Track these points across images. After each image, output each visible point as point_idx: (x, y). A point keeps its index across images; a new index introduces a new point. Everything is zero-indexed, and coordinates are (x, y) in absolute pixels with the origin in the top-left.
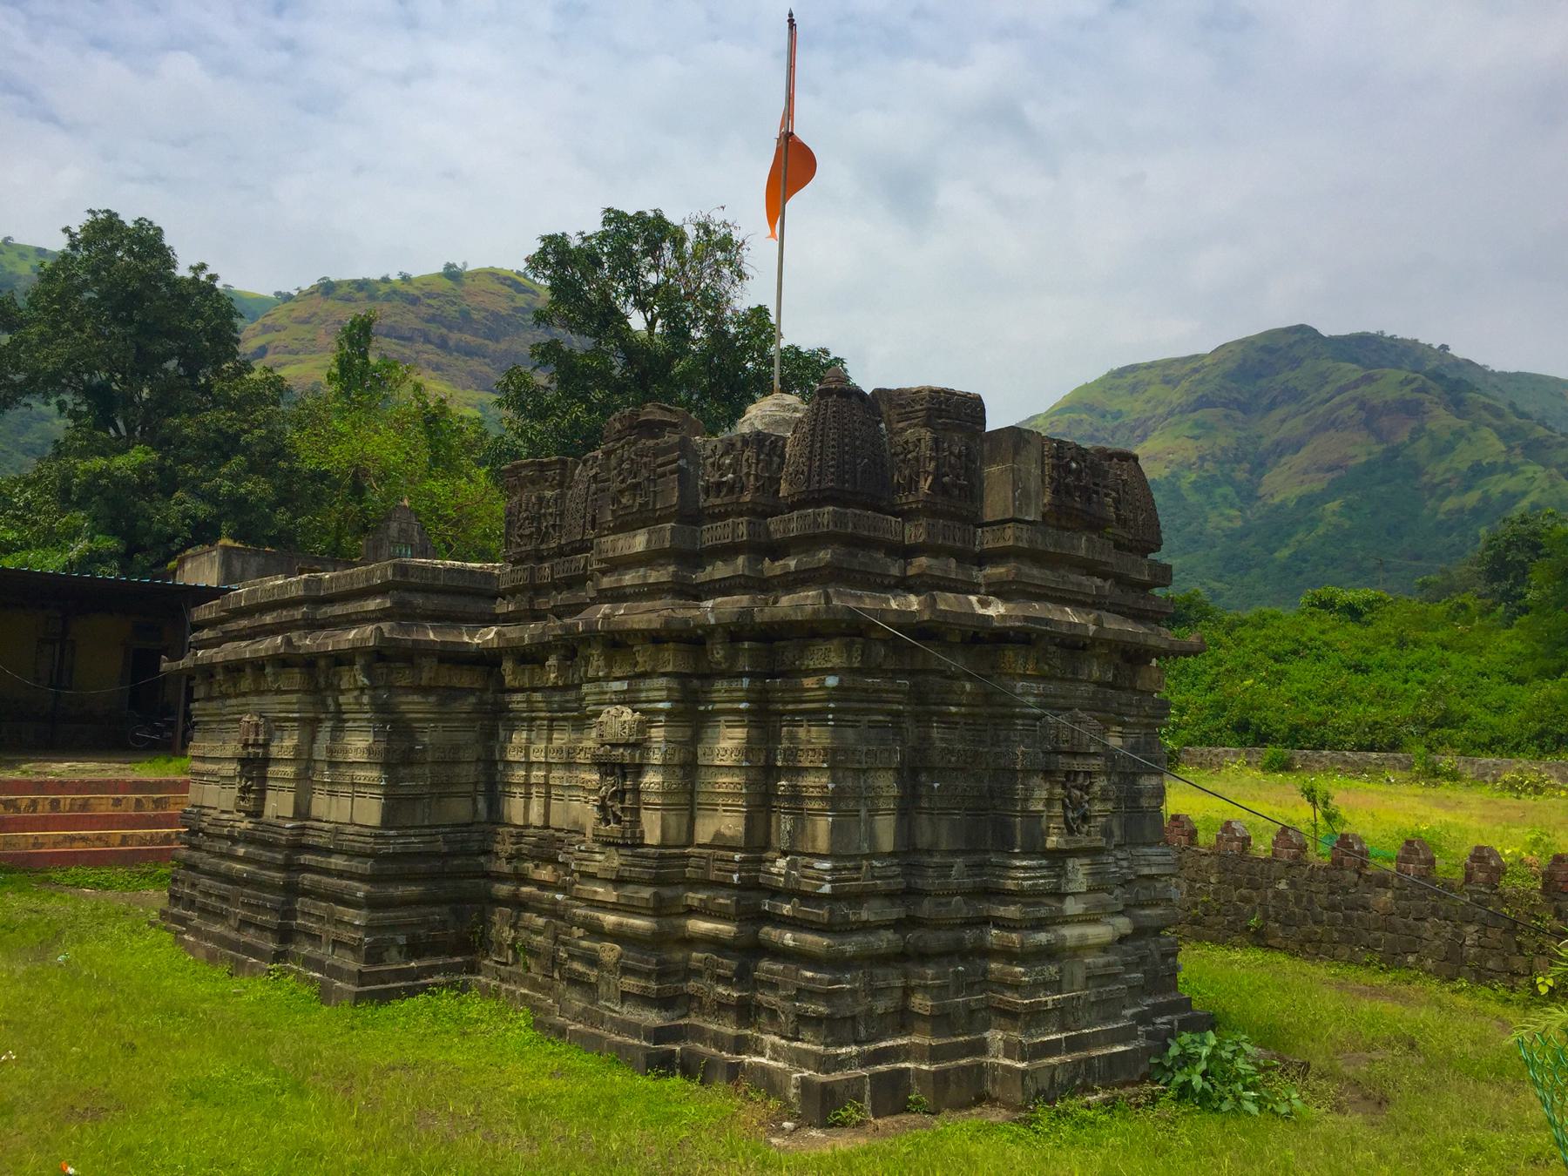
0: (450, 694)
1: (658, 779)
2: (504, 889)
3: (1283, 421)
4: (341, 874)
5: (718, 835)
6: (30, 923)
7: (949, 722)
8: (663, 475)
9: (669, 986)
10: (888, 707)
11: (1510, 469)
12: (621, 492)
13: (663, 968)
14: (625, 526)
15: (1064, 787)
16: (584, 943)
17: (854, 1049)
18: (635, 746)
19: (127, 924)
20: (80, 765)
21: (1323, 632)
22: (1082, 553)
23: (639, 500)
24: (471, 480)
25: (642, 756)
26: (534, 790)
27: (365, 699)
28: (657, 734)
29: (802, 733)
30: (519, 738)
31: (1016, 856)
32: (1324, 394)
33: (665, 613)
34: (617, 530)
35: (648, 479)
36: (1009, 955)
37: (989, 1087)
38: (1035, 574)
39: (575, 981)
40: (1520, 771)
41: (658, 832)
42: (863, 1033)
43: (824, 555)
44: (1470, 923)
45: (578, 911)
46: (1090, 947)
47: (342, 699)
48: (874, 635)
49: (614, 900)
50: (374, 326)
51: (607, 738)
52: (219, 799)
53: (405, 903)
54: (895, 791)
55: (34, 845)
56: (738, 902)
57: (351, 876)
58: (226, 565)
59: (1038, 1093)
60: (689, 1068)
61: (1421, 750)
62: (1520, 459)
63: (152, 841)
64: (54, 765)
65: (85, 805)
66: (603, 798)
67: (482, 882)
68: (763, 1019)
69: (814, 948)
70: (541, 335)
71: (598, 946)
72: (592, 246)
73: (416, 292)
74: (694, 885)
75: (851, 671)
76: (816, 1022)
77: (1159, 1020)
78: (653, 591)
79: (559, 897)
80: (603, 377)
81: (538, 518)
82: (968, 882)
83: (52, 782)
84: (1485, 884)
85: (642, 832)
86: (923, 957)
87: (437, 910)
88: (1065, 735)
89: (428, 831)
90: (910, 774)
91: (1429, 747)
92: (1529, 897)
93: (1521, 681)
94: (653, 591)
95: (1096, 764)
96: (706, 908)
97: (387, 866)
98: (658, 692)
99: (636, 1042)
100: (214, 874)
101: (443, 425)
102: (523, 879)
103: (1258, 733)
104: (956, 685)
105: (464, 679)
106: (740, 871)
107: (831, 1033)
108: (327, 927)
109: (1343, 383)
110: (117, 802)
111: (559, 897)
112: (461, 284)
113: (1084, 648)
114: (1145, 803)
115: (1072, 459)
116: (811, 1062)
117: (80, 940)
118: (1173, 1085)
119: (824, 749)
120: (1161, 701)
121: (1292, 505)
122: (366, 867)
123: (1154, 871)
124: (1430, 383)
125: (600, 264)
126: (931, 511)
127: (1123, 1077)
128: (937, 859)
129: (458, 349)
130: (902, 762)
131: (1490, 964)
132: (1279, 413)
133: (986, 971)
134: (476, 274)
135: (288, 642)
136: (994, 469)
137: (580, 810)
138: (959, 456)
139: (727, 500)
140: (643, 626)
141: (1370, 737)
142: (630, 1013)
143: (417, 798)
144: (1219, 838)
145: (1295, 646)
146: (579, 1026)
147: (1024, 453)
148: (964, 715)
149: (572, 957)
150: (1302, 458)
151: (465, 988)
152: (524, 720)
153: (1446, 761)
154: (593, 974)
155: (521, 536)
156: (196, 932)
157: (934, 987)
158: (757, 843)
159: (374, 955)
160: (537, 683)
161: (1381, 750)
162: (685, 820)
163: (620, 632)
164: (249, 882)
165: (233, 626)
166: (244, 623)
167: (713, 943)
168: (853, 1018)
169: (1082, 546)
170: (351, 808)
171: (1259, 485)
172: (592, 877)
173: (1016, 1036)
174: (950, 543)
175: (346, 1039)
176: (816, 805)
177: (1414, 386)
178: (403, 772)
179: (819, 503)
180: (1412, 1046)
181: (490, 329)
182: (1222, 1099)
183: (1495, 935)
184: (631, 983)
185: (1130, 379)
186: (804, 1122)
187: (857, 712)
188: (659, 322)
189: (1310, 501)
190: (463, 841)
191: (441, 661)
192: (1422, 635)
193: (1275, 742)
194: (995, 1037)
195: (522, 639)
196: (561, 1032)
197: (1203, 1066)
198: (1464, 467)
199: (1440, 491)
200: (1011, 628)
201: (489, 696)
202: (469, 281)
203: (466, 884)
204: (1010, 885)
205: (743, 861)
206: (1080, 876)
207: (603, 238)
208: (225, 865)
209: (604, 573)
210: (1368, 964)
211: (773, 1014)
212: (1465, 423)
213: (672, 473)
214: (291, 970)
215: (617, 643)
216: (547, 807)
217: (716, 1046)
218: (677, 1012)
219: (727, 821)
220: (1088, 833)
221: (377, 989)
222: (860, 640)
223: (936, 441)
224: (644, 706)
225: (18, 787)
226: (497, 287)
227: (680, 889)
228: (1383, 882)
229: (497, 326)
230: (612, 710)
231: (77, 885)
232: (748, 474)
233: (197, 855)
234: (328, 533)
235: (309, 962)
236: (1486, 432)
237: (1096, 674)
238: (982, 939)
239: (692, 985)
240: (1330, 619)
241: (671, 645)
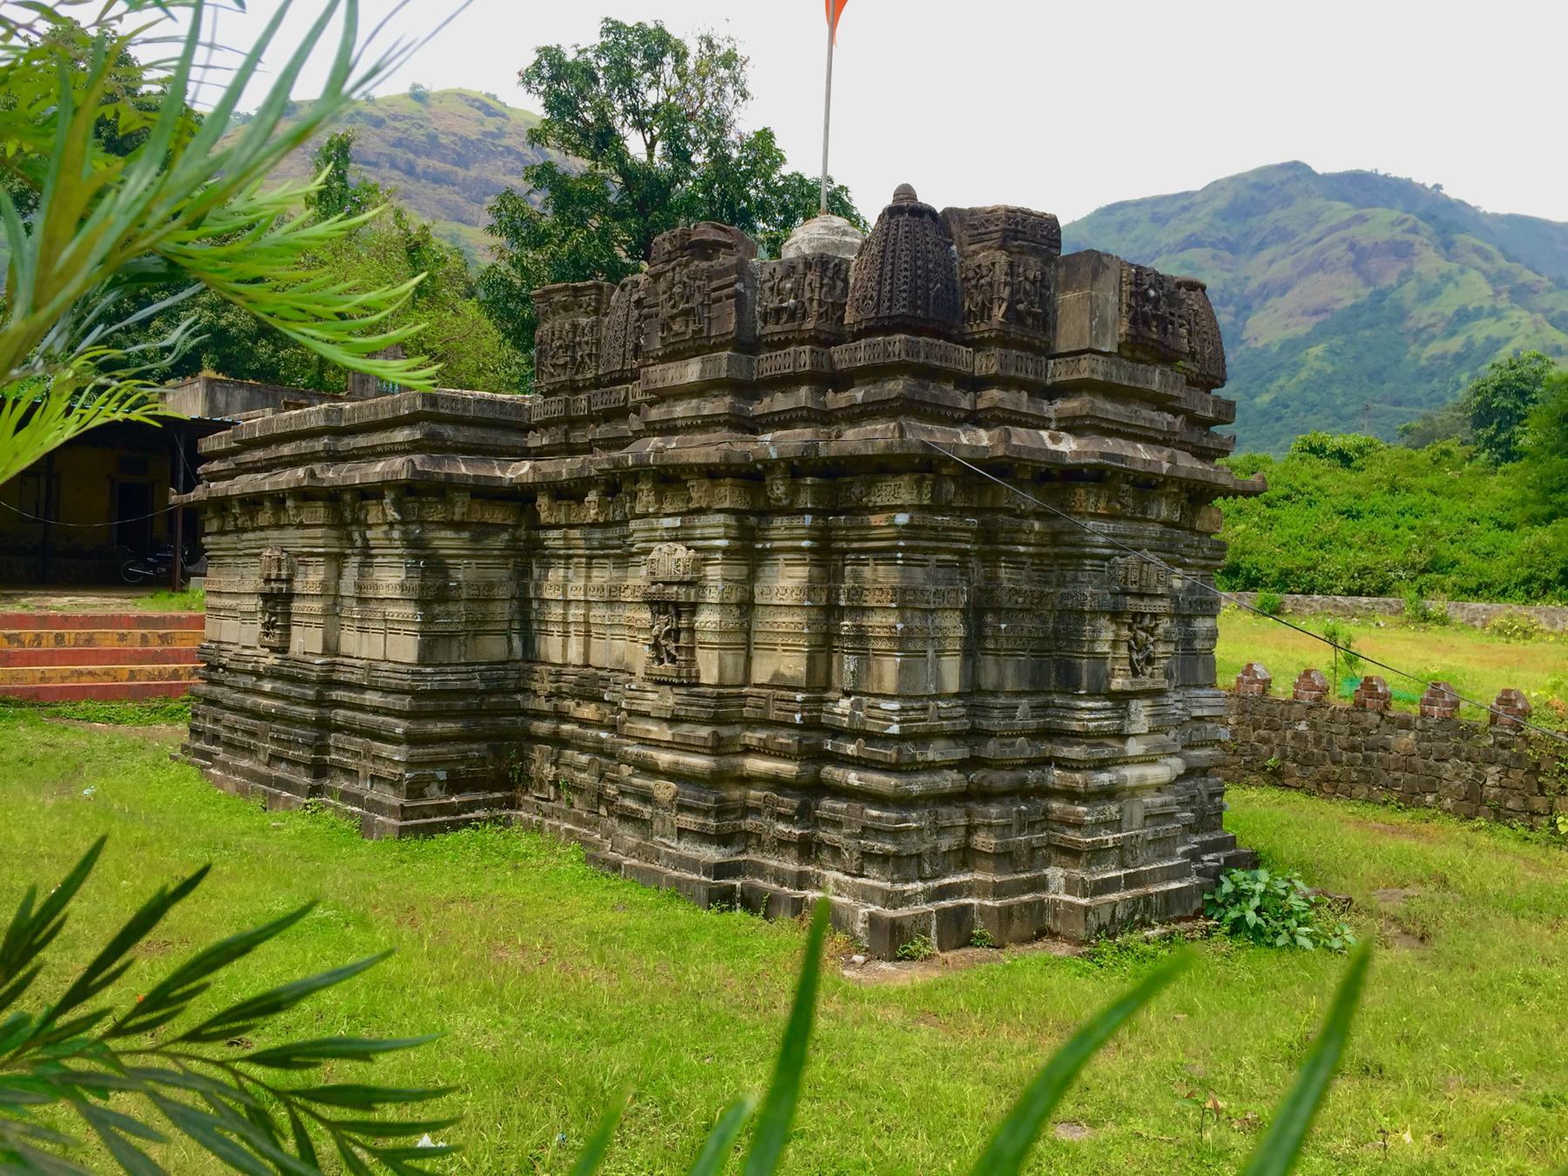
0: (483, 531)
1: (715, 617)
2: (544, 727)
3: (1271, 262)
4: (376, 710)
5: (777, 675)
6: (46, 758)
7: (1015, 560)
8: (719, 300)
9: (729, 823)
10: (955, 546)
11: (1496, 313)
12: (673, 318)
13: (720, 807)
14: (676, 354)
15: (1130, 629)
16: (636, 781)
17: (919, 886)
18: (690, 584)
19: (149, 757)
20: (81, 600)
21: (1316, 477)
22: (1155, 387)
23: (692, 327)
24: (457, 314)
25: (697, 593)
26: (572, 628)
27: (396, 534)
28: (714, 572)
29: (867, 572)
30: (556, 575)
31: (1080, 697)
32: (1314, 234)
33: (725, 446)
34: (665, 359)
35: (702, 304)
36: (1071, 795)
37: (1049, 922)
38: (1109, 409)
39: (627, 817)
40: (1510, 616)
41: (715, 672)
42: (928, 870)
43: (895, 387)
44: (1492, 764)
45: (630, 750)
46: (1148, 787)
47: (369, 534)
48: (944, 471)
49: (669, 738)
50: (353, 146)
51: (660, 576)
52: (241, 634)
53: (443, 739)
54: (961, 632)
55: (41, 679)
56: (800, 741)
57: (388, 712)
58: (210, 397)
59: (1099, 930)
60: (750, 901)
61: (1413, 594)
62: (1507, 304)
63: (160, 676)
64: (54, 600)
65: (89, 641)
66: (656, 637)
67: (519, 719)
68: (825, 855)
69: (880, 788)
70: (534, 157)
71: (651, 784)
72: (587, 61)
73: (382, 115)
74: (750, 724)
75: (921, 508)
76: (885, 858)
77: (1205, 858)
78: (707, 424)
79: (604, 735)
80: (596, 200)
81: (572, 347)
82: (1033, 723)
83: (55, 616)
84: (1510, 726)
85: (698, 672)
86: (987, 796)
87: (476, 746)
88: (1134, 575)
89: (464, 669)
90: (976, 614)
91: (1420, 591)
92: (1555, 739)
93: (1510, 527)
94: (707, 424)
95: (1162, 605)
96: (765, 747)
97: (427, 703)
98: (715, 530)
99: (695, 877)
100: (240, 710)
101: (427, 255)
102: (563, 717)
103: (1248, 578)
104: (1025, 525)
105: (496, 516)
106: (802, 710)
107: (898, 869)
108: (364, 762)
109: (1333, 222)
110: (122, 637)
111: (604, 735)
112: (429, 106)
113: (1154, 487)
114: (1198, 645)
115: (1151, 286)
116: (878, 898)
117: (104, 774)
118: (1226, 920)
119: (893, 588)
120: (1219, 542)
121: (1275, 349)
122: (406, 703)
123: (1206, 712)
124: (1421, 223)
125: (596, 81)
126: (1004, 341)
127: (1178, 913)
128: (1002, 701)
129: (426, 175)
130: (968, 603)
131: (1510, 804)
132: (1266, 254)
133: (1047, 811)
134: (444, 95)
135: (312, 475)
136: (1070, 296)
137: (626, 647)
138: (1033, 283)
139: (787, 327)
140: (700, 460)
141: (1358, 582)
142: (687, 849)
143: (452, 636)
144: (1239, 680)
145: (1287, 491)
146: (634, 861)
147: (1102, 279)
148: (1031, 555)
149: (623, 793)
150: (1289, 301)
151: (507, 823)
152: (559, 557)
153: (1436, 605)
154: (647, 811)
155: (554, 366)
156: (224, 766)
157: (999, 825)
158: (818, 685)
159: (415, 790)
160: (574, 520)
161: (1369, 594)
162: (742, 660)
163: (674, 466)
164: (274, 718)
165: (247, 457)
166: (259, 454)
167: (776, 783)
168: (919, 856)
169: (1155, 379)
170: (387, 643)
171: (1244, 328)
172: (645, 715)
173: (1078, 873)
174: (1022, 375)
175: (398, 871)
176: (883, 645)
177: (1405, 227)
178: (437, 609)
179: (888, 331)
180: (1444, 882)
181: (459, 155)
182: (1276, 934)
183: (1517, 776)
184: (689, 820)
185: (1118, 217)
186: (873, 954)
187: (925, 550)
188: (659, 145)
189: (1293, 346)
190: (498, 679)
191: (473, 496)
192: (1412, 480)
193: (1265, 585)
194: (1056, 874)
195: (560, 473)
196: (616, 867)
197: (1256, 902)
198: (1449, 312)
199: (1424, 336)
200: (1086, 465)
201: (522, 533)
202: (435, 103)
203: (504, 721)
204: (1075, 726)
205: (805, 701)
206: (1142, 717)
207: (603, 50)
208: (250, 701)
209: (651, 404)
210: (1385, 803)
211: (836, 851)
212: (1454, 266)
213: (728, 297)
214: (328, 805)
215: (669, 478)
216: (587, 646)
217: (777, 881)
218: (736, 849)
219: (787, 660)
220: (1152, 676)
221: (421, 824)
222: (930, 476)
223: (1011, 265)
224: (700, 543)
225: (21, 621)
226: (466, 109)
227: (738, 729)
228: (1406, 724)
229: (467, 150)
230: (665, 547)
231: (88, 719)
232: (811, 300)
233: (217, 690)
234: (309, 367)
235: (345, 796)
236: (1473, 275)
237: (1164, 513)
238: (1044, 779)
239: (749, 823)
240: (1321, 465)
241: (728, 481)
